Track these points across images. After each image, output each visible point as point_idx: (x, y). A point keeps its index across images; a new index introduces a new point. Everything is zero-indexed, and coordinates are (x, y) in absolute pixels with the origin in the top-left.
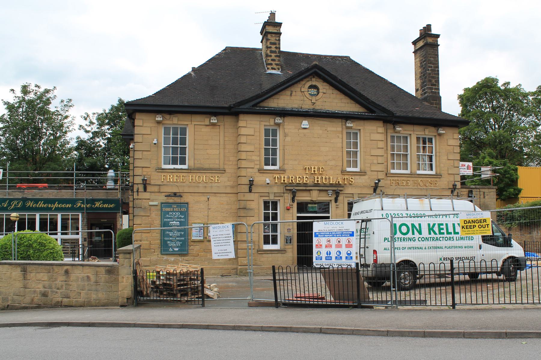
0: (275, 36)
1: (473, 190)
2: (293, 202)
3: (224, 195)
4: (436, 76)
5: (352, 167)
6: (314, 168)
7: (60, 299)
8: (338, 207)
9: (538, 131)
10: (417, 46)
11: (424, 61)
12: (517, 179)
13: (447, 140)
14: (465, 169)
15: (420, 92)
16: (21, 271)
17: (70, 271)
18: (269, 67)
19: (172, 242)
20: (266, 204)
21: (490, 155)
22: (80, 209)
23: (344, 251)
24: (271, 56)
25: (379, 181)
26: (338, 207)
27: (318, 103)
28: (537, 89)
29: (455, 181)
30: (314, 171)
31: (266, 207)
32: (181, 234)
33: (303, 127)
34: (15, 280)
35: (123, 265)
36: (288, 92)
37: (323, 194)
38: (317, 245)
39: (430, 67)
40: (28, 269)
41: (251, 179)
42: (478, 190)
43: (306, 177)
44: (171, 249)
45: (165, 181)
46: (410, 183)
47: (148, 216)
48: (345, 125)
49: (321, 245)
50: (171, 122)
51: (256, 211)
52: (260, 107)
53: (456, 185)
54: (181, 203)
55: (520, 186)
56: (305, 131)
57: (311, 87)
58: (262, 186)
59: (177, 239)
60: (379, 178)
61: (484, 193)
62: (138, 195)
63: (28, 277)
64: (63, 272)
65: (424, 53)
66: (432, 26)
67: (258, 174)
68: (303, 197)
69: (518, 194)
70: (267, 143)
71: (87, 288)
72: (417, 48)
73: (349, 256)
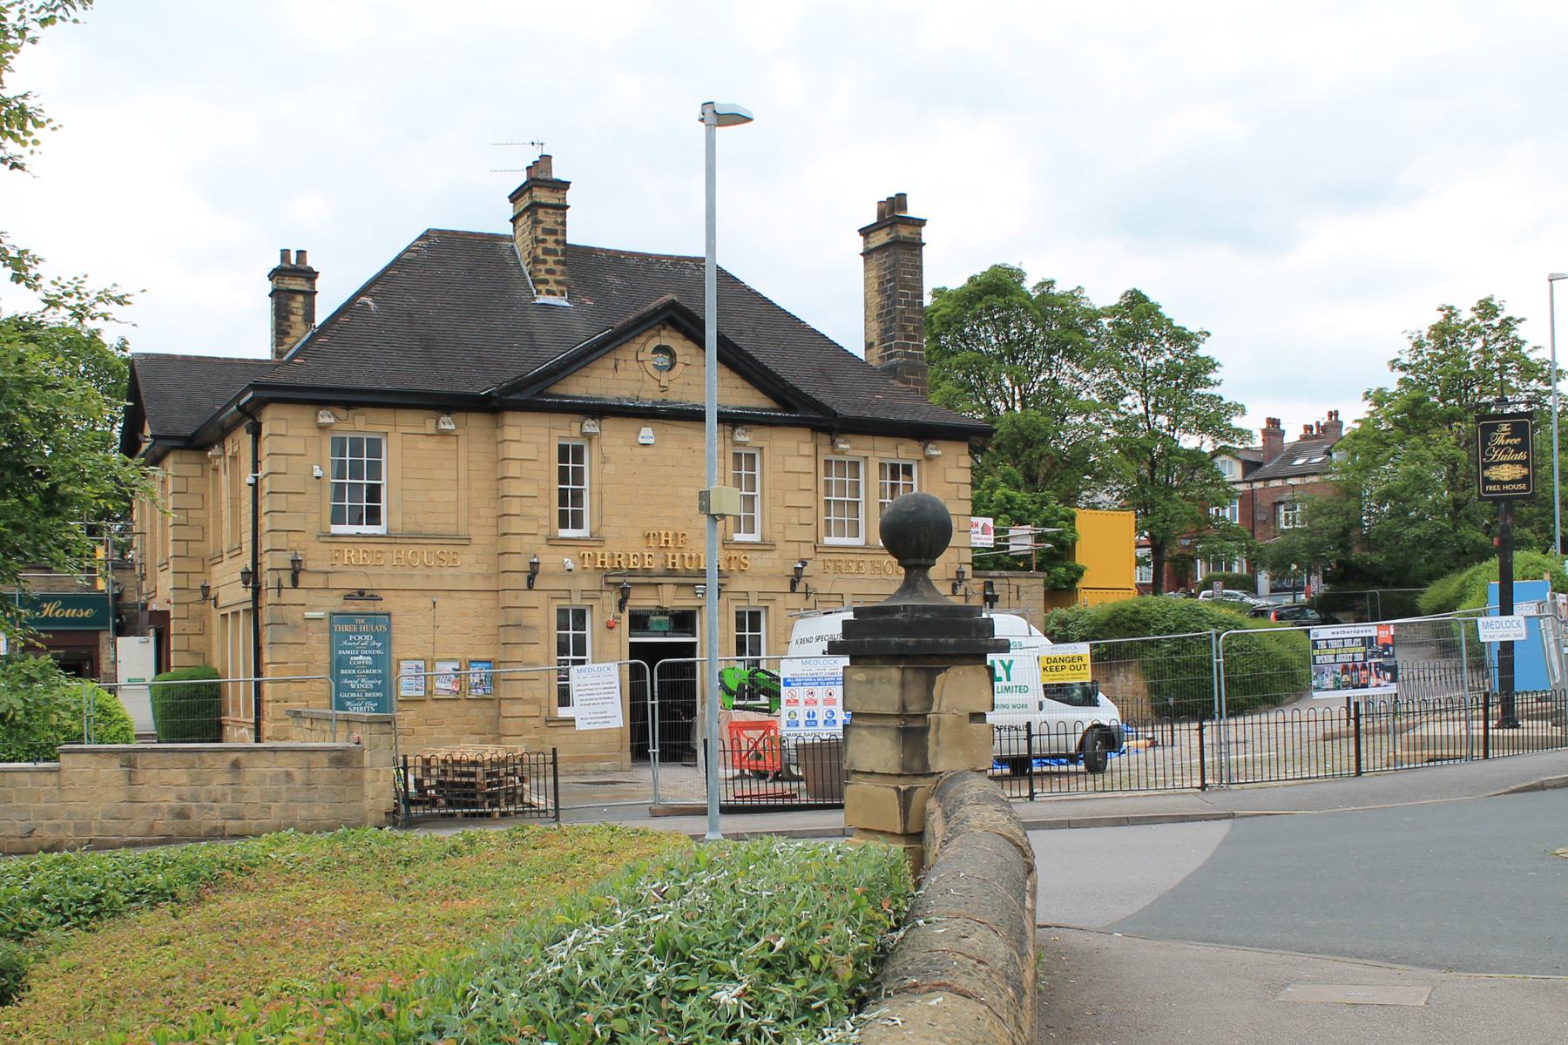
0: (553, 214)
1: (995, 581)
2: (621, 612)
3: (469, 595)
6: (667, 535)
7: (220, 823)
9: (1122, 409)
10: (871, 240)
11: (889, 281)
12: (1074, 541)
13: (945, 470)
14: (977, 533)
15: (877, 351)
16: (122, 766)
17: (243, 763)
18: (540, 287)
21: (1007, 479)
23: (821, 713)
24: (545, 262)
25: (804, 564)
27: (673, 388)
28: (1122, 297)
29: (961, 564)
30: (667, 542)
33: (642, 441)
34: (106, 785)
35: (378, 746)
36: (609, 362)
37: (686, 592)
38: (788, 701)
39: (902, 295)
40: (139, 761)
41: (535, 560)
42: (1006, 581)
43: (650, 556)
45: (338, 563)
46: (866, 567)
48: (732, 438)
49: (796, 701)
50: (350, 428)
51: (543, 631)
52: (550, 396)
53: (963, 573)
54: (375, 614)
55: (1080, 559)
57: (660, 349)
58: (553, 575)
60: (803, 556)
61: (1018, 588)
62: (279, 596)
63: (140, 776)
64: (227, 764)
65: (890, 262)
66: (908, 198)
67: (545, 548)
68: (642, 600)
69: (1074, 581)
70: (563, 474)
71: (285, 796)
72: (872, 246)
73: (830, 722)
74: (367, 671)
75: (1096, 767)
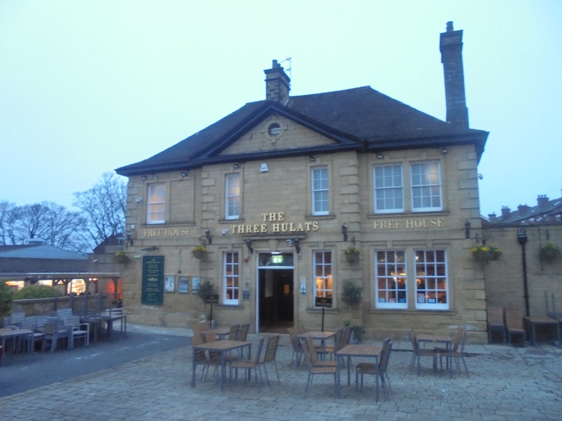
5: (431, 204)
8: (300, 258)
26: (300, 258)
33: (262, 170)
52: (221, 156)
56: (266, 174)
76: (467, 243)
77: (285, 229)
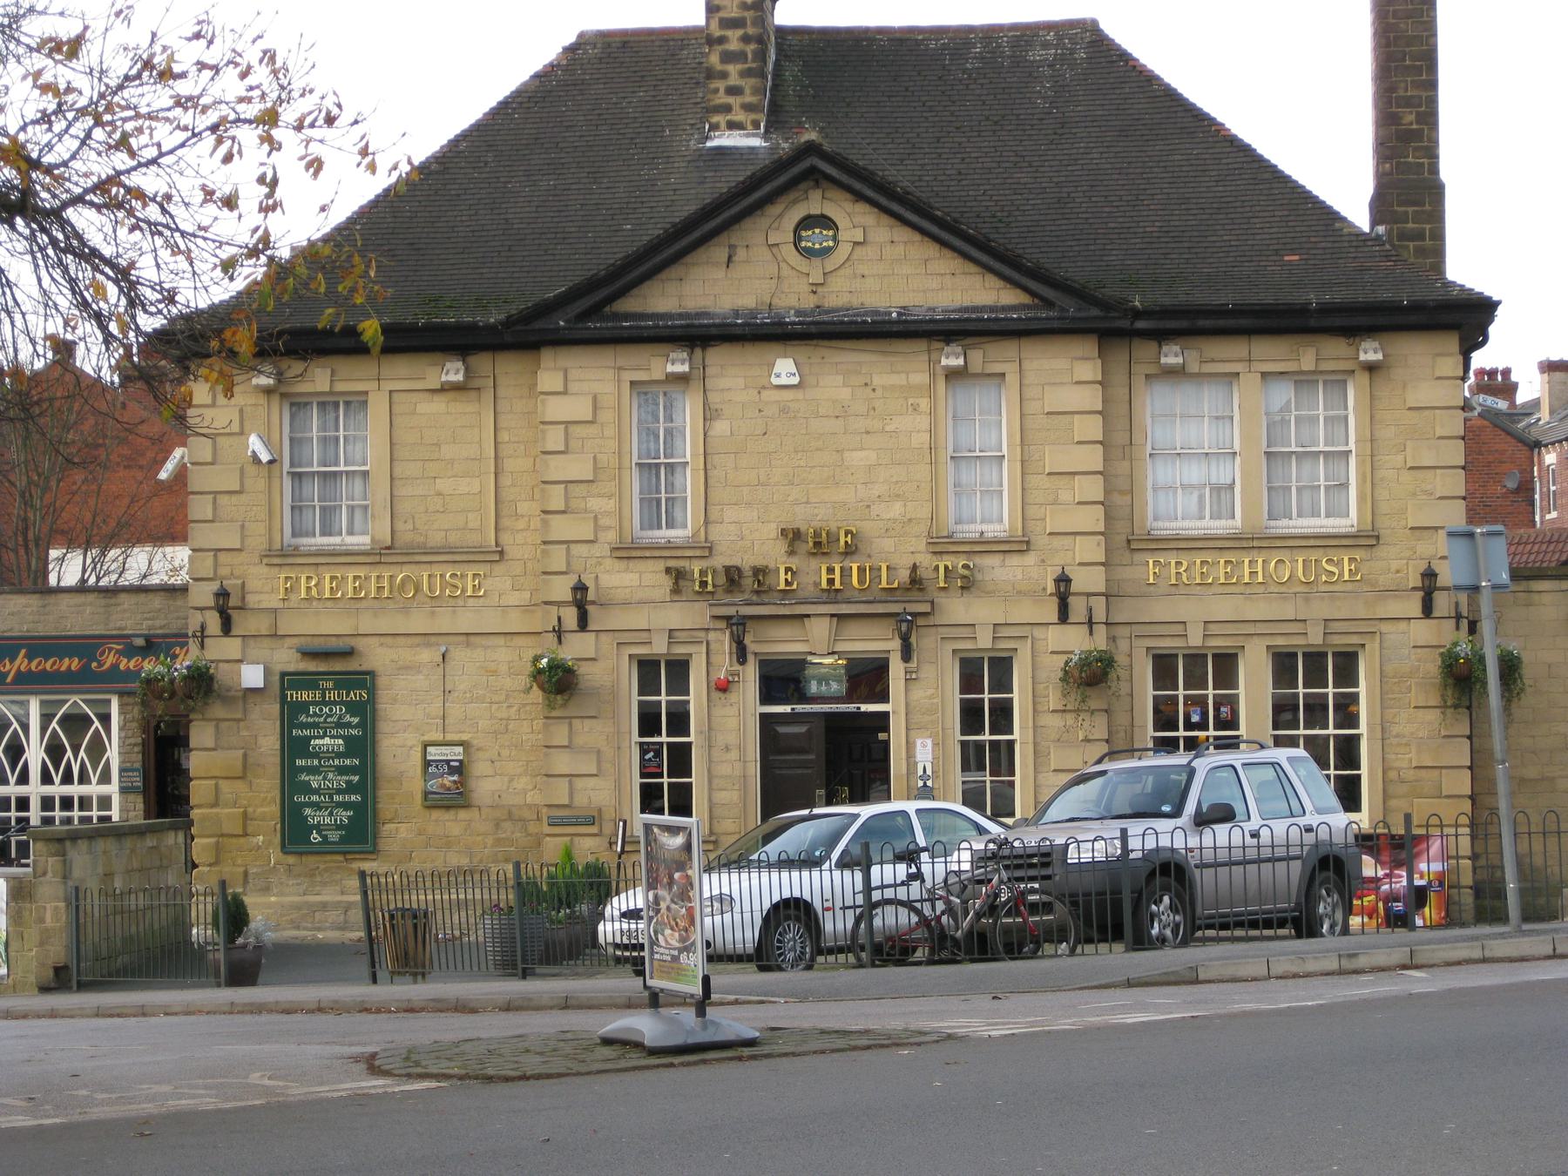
3: (501, 641)
4: (1424, 94)
19: (320, 809)
20: (647, 669)
22: (111, 679)
26: (914, 676)
31: (648, 682)
32: (348, 783)
33: (775, 381)
36: (718, 251)
44: (315, 837)
47: (239, 720)
57: (808, 222)
59: (336, 798)
74: (337, 762)
75: (1304, 925)
76: (1423, 631)
77: (861, 581)
